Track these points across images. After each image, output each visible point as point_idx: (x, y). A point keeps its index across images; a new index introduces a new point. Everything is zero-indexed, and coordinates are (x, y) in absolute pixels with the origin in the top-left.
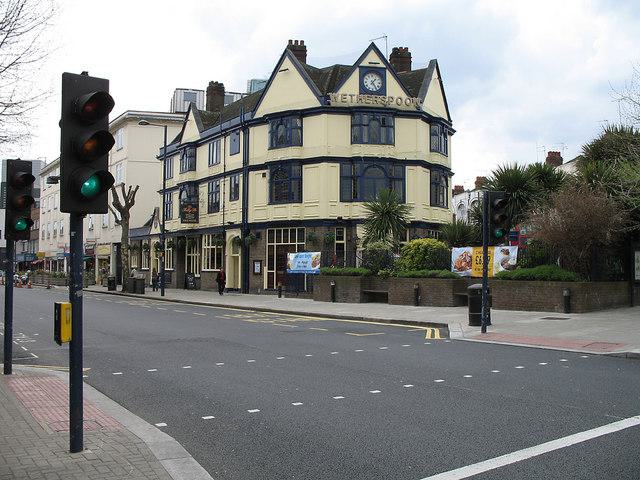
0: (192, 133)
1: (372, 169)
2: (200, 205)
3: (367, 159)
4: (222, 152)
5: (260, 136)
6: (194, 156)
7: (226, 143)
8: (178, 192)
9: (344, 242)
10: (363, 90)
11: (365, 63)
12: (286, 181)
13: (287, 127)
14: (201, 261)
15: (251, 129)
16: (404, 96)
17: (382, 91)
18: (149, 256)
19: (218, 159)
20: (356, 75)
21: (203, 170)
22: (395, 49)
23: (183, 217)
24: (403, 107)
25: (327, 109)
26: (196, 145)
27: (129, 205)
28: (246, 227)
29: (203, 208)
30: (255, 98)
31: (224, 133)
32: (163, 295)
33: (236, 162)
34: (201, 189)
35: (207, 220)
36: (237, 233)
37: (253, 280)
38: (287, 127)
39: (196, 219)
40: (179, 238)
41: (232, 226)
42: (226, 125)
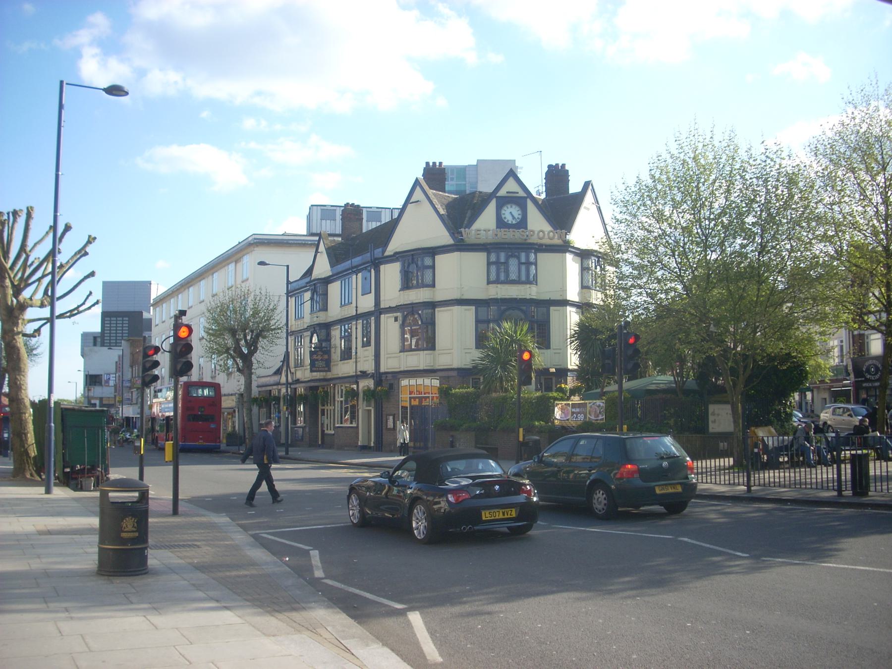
0: (323, 268)
1: (511, 311)
2: (333, 350)
3: (504, 301)
4: (354, 291)
5: (391, 274)
6: (325, 294)
7: (357, 280)
8: (309, 333)
9: (98, 408)
10: (501, 223)
11: (502, 192)
12: (420, 323)
13: (417, 264)
14: (333, 419)
15: (382, 267)
16: (547, 227)
17: (522, 224)
18: (279, 407)
19: (347, 298)
20: (492, 207)
21: (335, 311)
22: (550, 166)
23: (313, 367)
24: (546, 241)
25: (460, 246)
26: (327, 281)
27: (252, 353)
28: (379, 377)
29: (336, 355)
30: (388, 230)
31: (355, 270)
32: (287, 453)
33: (367, 303)
34: (333, 333)
35: (344, 369)
36: (369, 383)
37: (387, 437)
38: (417, 264)
39: (328, 366)
40: (311, 388)
41: (364, 375)
42: (357, 260)
